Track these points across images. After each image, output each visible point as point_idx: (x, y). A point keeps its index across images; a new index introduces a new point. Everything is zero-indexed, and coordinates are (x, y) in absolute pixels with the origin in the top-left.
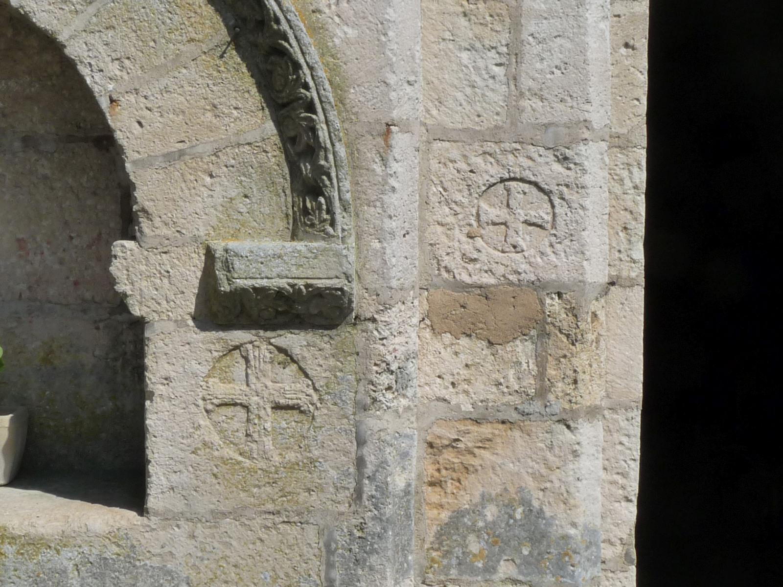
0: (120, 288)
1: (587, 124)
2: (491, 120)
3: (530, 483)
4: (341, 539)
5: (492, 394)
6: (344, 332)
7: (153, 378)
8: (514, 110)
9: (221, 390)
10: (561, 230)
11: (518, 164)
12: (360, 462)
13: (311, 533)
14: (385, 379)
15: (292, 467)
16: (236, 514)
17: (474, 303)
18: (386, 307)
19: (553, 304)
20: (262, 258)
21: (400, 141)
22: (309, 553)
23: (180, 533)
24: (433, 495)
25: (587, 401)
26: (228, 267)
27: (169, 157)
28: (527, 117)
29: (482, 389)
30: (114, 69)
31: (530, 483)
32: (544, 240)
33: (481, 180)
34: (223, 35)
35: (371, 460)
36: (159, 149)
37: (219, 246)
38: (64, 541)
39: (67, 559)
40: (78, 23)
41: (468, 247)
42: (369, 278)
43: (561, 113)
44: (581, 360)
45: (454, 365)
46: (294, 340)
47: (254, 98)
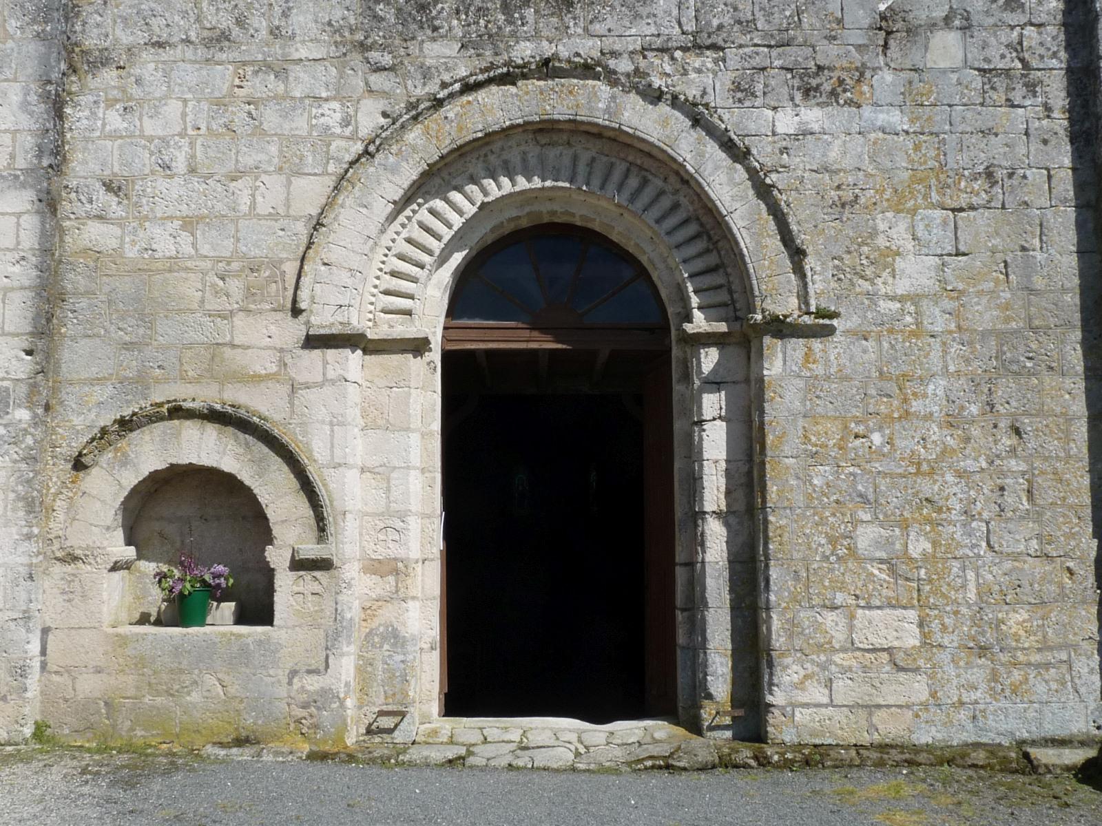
0: (268, 559)
1: (410, 511)
2: (381, 510)
3: (394, 619)
4: (330, 633)
5: (382, 592)
6: (332, 571)
7: (276, 586)
8: (388, 507)
9: (296, 589)
10: (402, 542)
11: (389, 523)
12: (336, 610)
13: (322, 630)
14: (344, 585)
15: (316, 611)
16: (300, 626)
17: (376, 564)
18: (344, 564)
19: (400, 565)
20: (33, 435)
21: (348, 515)
22: (321, 637)
23: (283, 632)
24: (364, 624)
25: (411, 594)
26: (298, 552)
27: (283, 522)
28: (392, 509)
29: (379, 591)
30: (267, 496)
31: (394, 619)
32: (397, 546)
33: (378, 528)
34: (298, 486)
35: (339, 609)
36: (280, 519)
37: (296, 547)
38: (249, 635)
39: (250, 640)
40: (257, 484)
41: (374, 548)
42: (339, 556)
43: (402, 507)
44: (409, 581)
45: (370, 584)
46: (318, 574)
47: (307, 504)
